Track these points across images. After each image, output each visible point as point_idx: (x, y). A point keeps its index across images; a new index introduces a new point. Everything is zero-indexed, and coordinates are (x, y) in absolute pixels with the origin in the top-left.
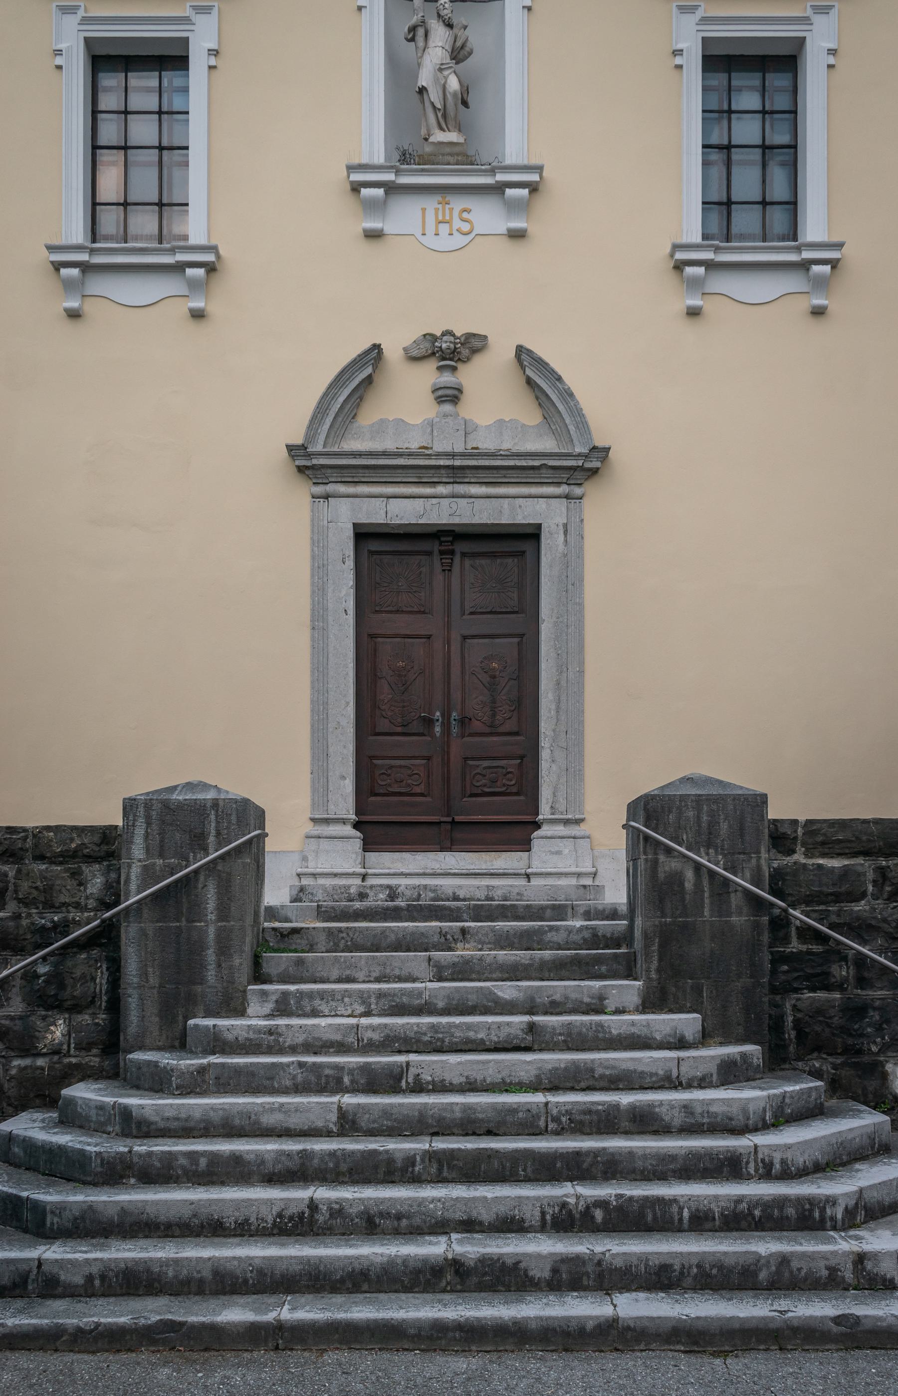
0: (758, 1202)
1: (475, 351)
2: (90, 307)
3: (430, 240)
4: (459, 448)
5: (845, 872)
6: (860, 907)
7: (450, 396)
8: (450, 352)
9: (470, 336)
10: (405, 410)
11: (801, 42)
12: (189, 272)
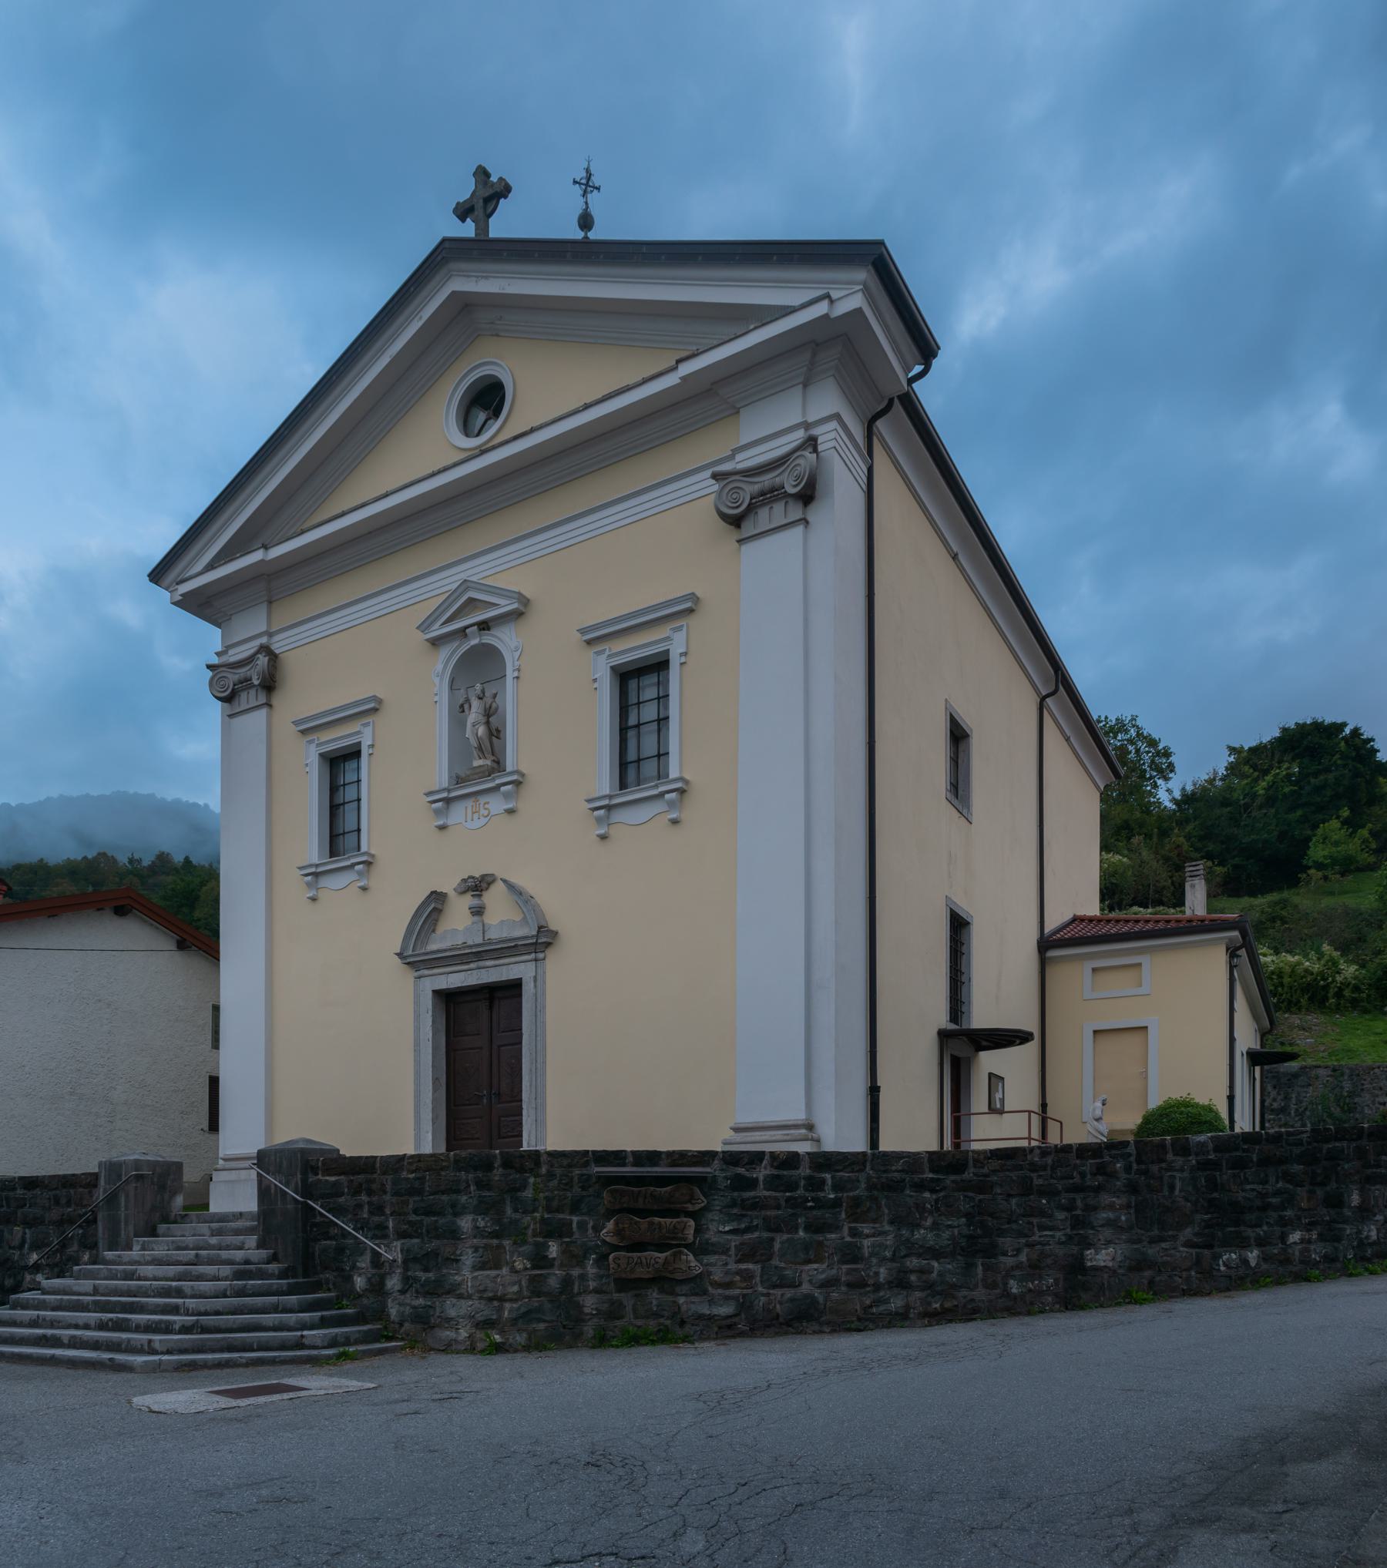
0: (154, 1322)
1: (489, 884)
2: (613, 831)
3: (469, 825)
4: (479, 940)
5: (335, 1183)
6: (342, 1200)
7: (478, 911)
8: (477, 886)
9: (484, 877)
10: (457, 925)
11: (359, 743)
12: (667, 796)
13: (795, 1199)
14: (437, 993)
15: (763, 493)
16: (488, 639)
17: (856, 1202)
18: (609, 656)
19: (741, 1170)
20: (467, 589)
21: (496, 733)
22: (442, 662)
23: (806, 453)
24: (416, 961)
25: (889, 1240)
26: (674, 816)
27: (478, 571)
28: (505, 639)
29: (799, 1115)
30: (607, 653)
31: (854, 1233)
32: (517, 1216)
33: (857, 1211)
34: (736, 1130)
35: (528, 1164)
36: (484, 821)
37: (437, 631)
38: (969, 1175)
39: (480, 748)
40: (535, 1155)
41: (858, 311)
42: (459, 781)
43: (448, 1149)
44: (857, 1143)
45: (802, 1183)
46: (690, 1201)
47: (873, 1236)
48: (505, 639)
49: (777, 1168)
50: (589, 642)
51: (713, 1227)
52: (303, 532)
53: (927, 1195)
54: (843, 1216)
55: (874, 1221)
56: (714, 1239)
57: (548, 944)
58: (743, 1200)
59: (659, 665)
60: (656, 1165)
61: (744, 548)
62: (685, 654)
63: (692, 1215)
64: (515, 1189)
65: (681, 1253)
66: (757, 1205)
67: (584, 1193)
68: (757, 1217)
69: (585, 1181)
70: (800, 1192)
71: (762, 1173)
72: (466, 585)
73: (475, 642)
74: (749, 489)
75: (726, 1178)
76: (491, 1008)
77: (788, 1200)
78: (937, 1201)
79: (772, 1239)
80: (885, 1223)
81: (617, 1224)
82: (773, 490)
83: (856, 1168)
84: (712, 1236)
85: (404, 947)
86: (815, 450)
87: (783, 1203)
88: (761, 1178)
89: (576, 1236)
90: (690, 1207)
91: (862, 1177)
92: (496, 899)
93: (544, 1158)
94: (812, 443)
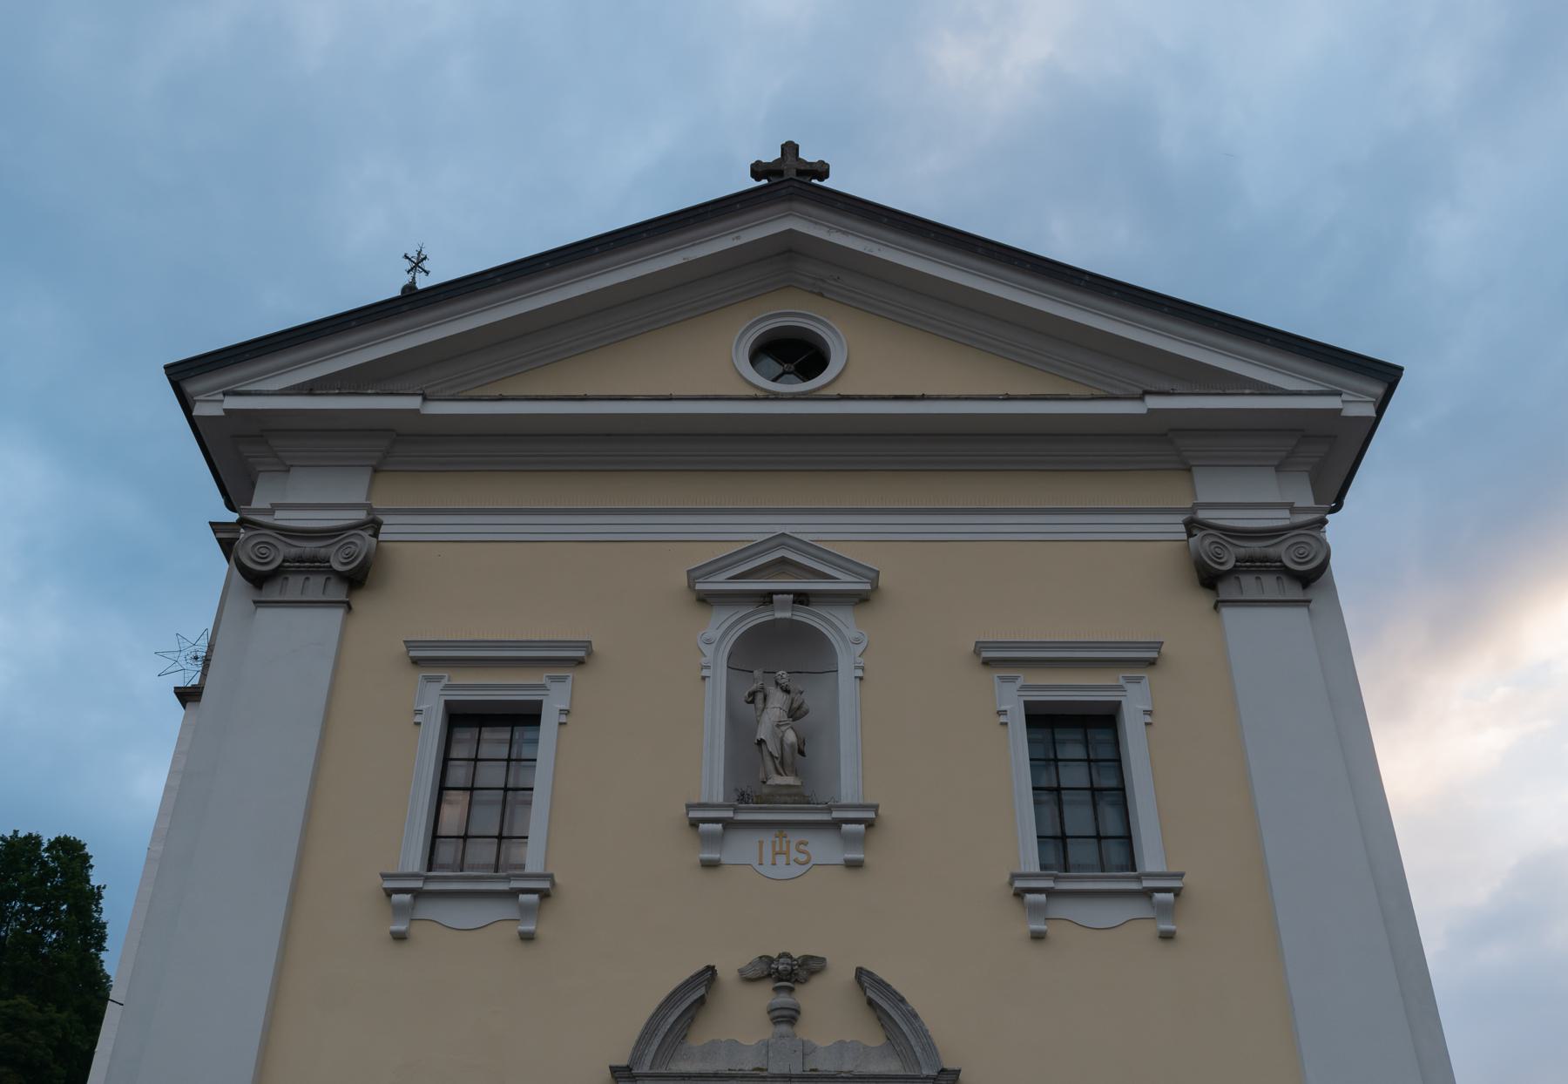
1: (813, 973)
3: (767, 870)
7: (787, 1017)
8: (788, 973)
9: (807, 959)
12: (523, 897)
15: (300, 559)
16: (803, 616)
18: (447, 687)
22: (721, 630)
23: (365, 534)
26: (1166, 927)
27: (807, 529)
28: (840, 626)
30: (445, 681)
36: (797, 870)
48: (840, 626)
50: (416, 662)
52: (501, 399)
59: (526, 717)
61: (260, 611)
62: (567, 712)
82: (313, 559)
86: (376, 535)
94: (374, 526)
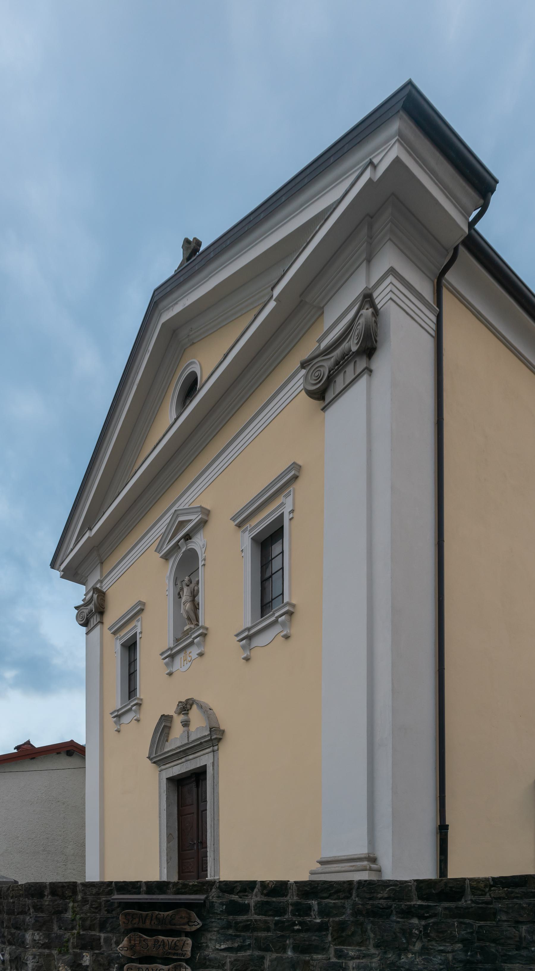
4: (186, 741)
7: (186, 724)
10: (177, 736)
13: (283, 922)
14: (169, 779)
17: (342, 927)
19: (235, 897)
20: (177, 516)
21: (196, 607)
24: (160, 760)
25: (375, 962)
29: (362, 850)
31: (340, 954)
32: (61, 932)
33: (342, 935)
34: (322, 863)
35: (68, 893)
36: (189, 664)
37: (166, 548)
38: (467, 901)
39: (189, 619)
40: (212, 884)
41: (397, 161)
42: (177, 640)
43: (179, 879)
44: (427, 871)
45: (290, 908)
46: (188, 923)
47: (358, 958)
49: (267, 895)
51: (211, 945)
53: (415, 921)
54: (330, 938)
55: (360, 944)
56: (212, 956)
57: (219, 740)
58: (237, 923)
60: (164, 893)
63: (187, 934)
64: (59, 912)
65: (181, 966)
66: (247, 927)
67: (109, 915)
68: (249, 938)
69: (110, 907)
70: (288, 916)
71: (253, 899)
72: (176, 514)
73: (183, 550)
74: (327, 364)
75: (222, 904)
76: (198, 786)
77: (277, 923)
78: (426, 927)
79: (263, 958)
80: (371, 947)
81: (130, 941)
83: (342, 895)
84: (210, 953)
85: (150, 753)
87: (272, 926)
88: (252, 904)
89: (104, 949)
90: (188, 929)
91: (348, 904)
92: (195, 714)
93: (79, 888)
